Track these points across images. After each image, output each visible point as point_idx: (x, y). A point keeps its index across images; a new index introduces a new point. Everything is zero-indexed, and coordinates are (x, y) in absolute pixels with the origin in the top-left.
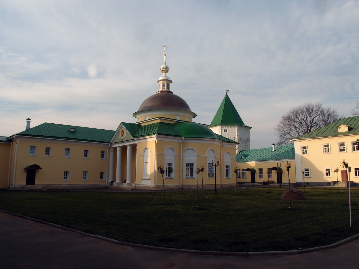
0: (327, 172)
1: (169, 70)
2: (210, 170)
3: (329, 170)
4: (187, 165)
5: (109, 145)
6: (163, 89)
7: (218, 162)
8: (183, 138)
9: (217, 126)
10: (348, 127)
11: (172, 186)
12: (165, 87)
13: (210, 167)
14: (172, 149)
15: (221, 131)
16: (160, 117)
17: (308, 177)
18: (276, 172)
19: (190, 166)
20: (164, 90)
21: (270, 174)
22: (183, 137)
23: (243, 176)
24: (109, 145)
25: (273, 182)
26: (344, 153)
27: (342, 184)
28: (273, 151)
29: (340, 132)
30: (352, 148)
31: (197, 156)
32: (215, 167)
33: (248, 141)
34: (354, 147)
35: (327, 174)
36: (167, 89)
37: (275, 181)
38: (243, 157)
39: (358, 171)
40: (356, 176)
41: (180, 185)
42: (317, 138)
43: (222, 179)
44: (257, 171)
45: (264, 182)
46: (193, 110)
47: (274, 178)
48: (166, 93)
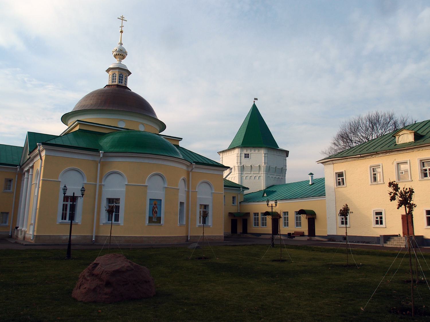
0: (377, 218)
1: (127, 55)
2: (153, 210)
3: (381, 213)
4: (110, 201)
6: (113, 82)
8: (102, 153)
9: (235, 149)
10: (413, 134)
11: (72, 237)
12: (115, 79)
13: (153, 205)
14: (209, 184)
15: (240, 156)
16: (78, 121)
17: (381, 226)
18: (306, 218)
20: (114, 83)
21: (299, 222)
22: (100, 152)
23: (262, 225)
24: (18, 170)
25: (302, 234)
27: (401, 241)
28: (310, 185)
29: (399, 143)
31: (126, 185)
33: (283, 171)
35: (377, 223)
36: (119, 82)
38: (265, 195)
42: (359, 156)
43: (189, 229)
45: (289, 234)
46: (160, 116)
47: (304, 228)
48: (115, 87)
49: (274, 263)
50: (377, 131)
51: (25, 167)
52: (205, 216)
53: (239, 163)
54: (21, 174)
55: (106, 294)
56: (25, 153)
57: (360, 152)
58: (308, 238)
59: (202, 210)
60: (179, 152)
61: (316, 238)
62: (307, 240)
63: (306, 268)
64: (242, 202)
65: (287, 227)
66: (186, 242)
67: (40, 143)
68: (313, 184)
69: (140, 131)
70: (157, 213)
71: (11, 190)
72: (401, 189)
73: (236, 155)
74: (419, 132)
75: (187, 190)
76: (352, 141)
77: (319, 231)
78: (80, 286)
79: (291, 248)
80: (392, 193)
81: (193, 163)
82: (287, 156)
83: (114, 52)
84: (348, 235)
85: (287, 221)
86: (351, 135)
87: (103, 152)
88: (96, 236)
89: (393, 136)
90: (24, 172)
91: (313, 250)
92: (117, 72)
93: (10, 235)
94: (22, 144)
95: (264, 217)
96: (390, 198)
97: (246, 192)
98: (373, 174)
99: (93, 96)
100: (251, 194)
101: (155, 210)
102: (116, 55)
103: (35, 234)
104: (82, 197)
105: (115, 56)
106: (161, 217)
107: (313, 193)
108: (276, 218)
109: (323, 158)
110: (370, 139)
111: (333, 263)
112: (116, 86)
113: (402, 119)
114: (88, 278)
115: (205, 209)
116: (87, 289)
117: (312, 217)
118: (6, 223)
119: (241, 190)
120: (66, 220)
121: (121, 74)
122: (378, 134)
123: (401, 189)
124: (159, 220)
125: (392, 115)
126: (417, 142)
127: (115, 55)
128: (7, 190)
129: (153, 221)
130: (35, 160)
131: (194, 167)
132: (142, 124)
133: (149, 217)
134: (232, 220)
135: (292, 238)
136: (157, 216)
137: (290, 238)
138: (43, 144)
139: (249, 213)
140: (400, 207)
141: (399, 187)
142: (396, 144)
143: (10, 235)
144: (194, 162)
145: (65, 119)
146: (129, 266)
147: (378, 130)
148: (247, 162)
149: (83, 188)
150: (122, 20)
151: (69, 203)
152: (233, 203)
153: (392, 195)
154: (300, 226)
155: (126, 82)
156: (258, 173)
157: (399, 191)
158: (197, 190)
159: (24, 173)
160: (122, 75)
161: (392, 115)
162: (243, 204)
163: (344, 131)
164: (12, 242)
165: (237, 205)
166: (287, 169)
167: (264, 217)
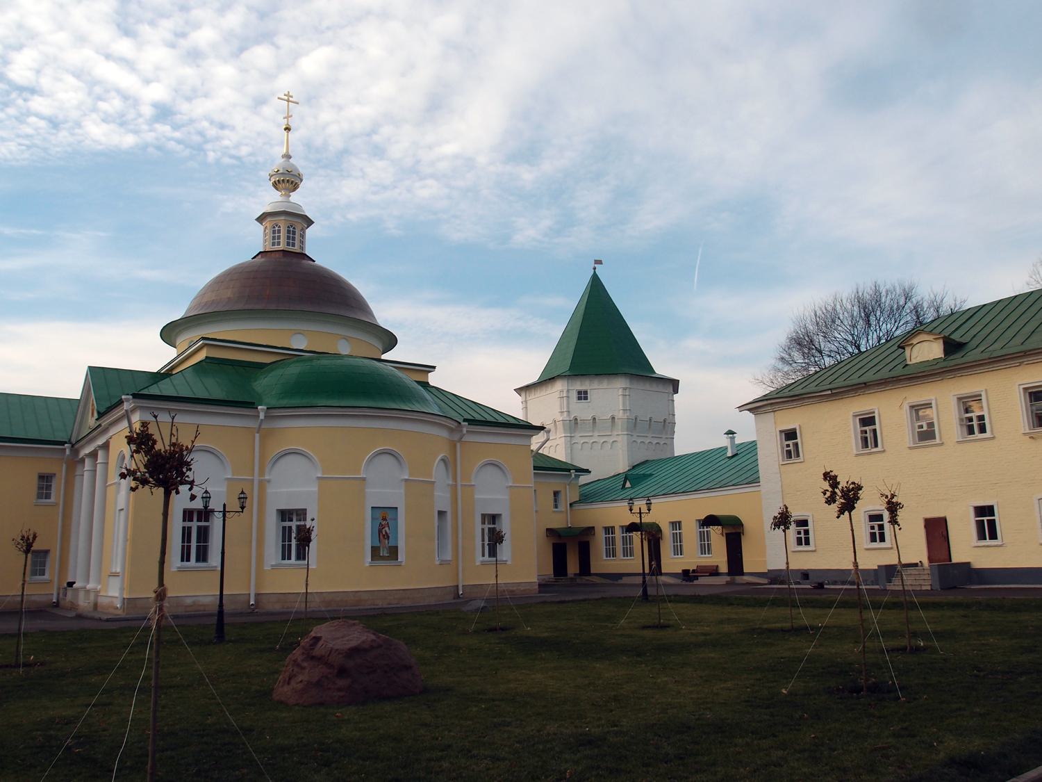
0: (872, 528)
1: (301, 180)
2: (380, 531)
4: (285, 515)
5: (65, 452)
6: (273, 244)
7: (243, 498)
12: (279, 237)
14: (498, 466)
16: (203, 338)
17: (882, 545)
19: (195, 518)
20: (276, 248)
21: (706, 543)
22: (259, 407)
24: (68, 452)
25: (714, 572)
26: (800, 431)
28: (729, 457)
29: (914, 361)
30: (961, 425)
31: (318, 478)
32: (224, 520)
33: (667, 426)
34: (971, 419)
35: (873, 538)
36: (288, 244)
37: (719, 565)
38: (628, 484)
39: (988, 520)
40: (982, 543)
41: (457, 586)
44: (667, 531)
45: (686, 572)
47: (719, 557)
49: (648, 633)
50: (878, 327)
51: (83, 447)
52: (495, 539)
53: (565, 414)
54: (75, 462)
55: (339, 690)
56: (84, 413)
57: (830, 384)
58: (728, 578)
59: (487, 526)
60: (430, 399)
61: (746, 579)
62: (699, 578)
63: (708, 637)
64: (575, 502)
65: (680, 556)
66: (454, 599)
67: (128, 395)
68: (736, 455)
69: (338, 356)
70: (388, 537)
71: (53, 499)
72: (843, 484)
73: (558, 393)
74: (956, 337)
75: (450, 482)
76: (820, 352)
77: (751, 564)
78: (290, 679)
79: (684, 602)
80: (828, 491)
81: (463, 423)
82: (676, 391)
83: (272, 176)
84: (791, 567)
85: (680, 542)
86: (819, 340)
87: (265, 408)
88: (257, 595)
89: (899, 347)
90: (80, 457)
91: (731, 604)
92: (283, 223)
93: (54, 602)
94: (76, 395)
95: (628, 534)
96: (824, 500)
97: (584, 479)
98: (859, 432)
99: (231, 280)
100: (596, 483)
101: (384, 530)
102: (277, 183)
103: (125, 597)
104: (242, 512)
105: (275, 185)
106: (397, 547)
107: (735, 476)
108: (653, 535)
109: (751, 400)
110: (863, 349)
111: (765, 626)
112: (282, 255)
113: (932, 296)
114: (305, 664)
115: (494, 523)
116: (306, 683)
117: (733, 531)
118: (44, 575)
119: (573, 476)
120: (189, 561)
121: (292, 226)
122: (881, 334)
123: (843, 484)
124: (394, 552)
125: (911, 289)
126: (952, 357)
127: (275, 182)
128: (42, 498)
129: (381, 555)
130: (112, 432)
131: (465, 432)
132: (344, 338)
133: (372, 547)
134: (554, 545)
135: (693, 581)
136: (390, 545)
137: (687, 581)
138: (135, 396)
139: (593, 528)
140: (842, 515)
141: (838, 480)
142: (907, 365)
143: (54, 601)
144: (465, 420)
145: (169, 333)
146: (373, 641)
147: (881, 324)
148: (583, 411)
149: (242, 493)
150: (288, 101)
151: (195, 525)
152: (556, 506)
153: (828, 494)
154: (709, 554)
155: (302, 242)
156: (610, 434)
157: (840, 487)
158: (473, 484)
159: (83, 460)
160: (294, 228)
161: (911, 289)
162: (577, 508)
163: (802, 330)
164: (70, 616)
165: (563, 510)
166: (676, 421)
167: (626, 536)
